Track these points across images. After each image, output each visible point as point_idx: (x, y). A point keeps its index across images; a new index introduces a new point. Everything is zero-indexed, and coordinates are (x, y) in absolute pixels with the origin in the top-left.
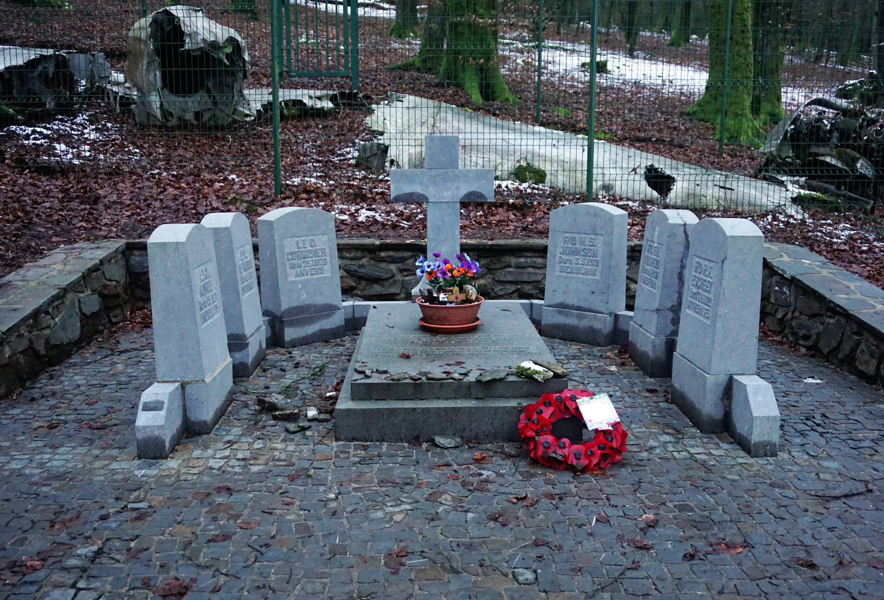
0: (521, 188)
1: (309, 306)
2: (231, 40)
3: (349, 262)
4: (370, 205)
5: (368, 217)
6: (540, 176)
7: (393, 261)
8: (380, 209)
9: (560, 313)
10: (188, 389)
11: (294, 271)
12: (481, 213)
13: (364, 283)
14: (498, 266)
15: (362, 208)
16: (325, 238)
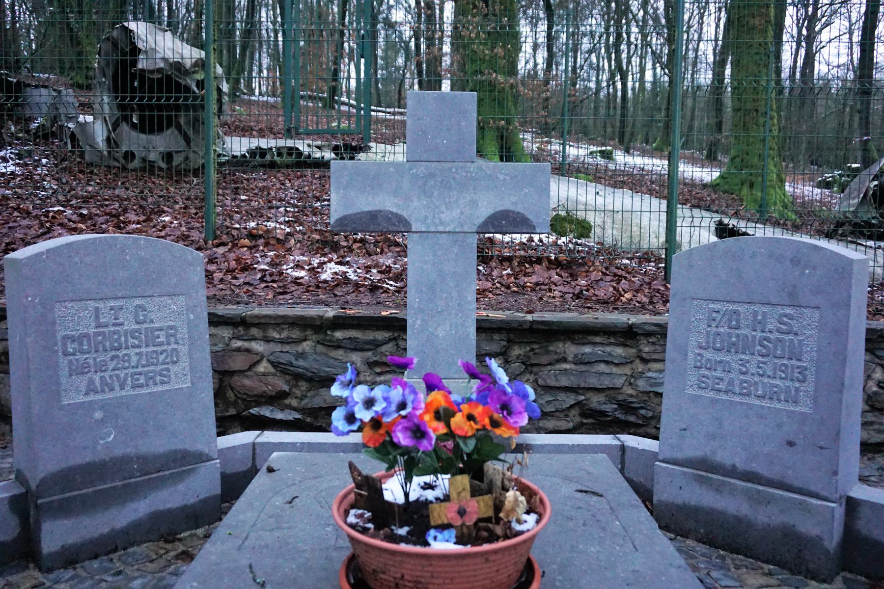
0: (559, 242)
1: (126, 460)
3: (278, 348)
4: (343, 257)
5: (336, 273)
6: (584, 229)
7: (357, 346)
8: (356, 262)
9: (701, 480)
11: (82, 382)
12: (509, 271)
13: (304, 385)
14: (544, 360)
15: (330, 261)
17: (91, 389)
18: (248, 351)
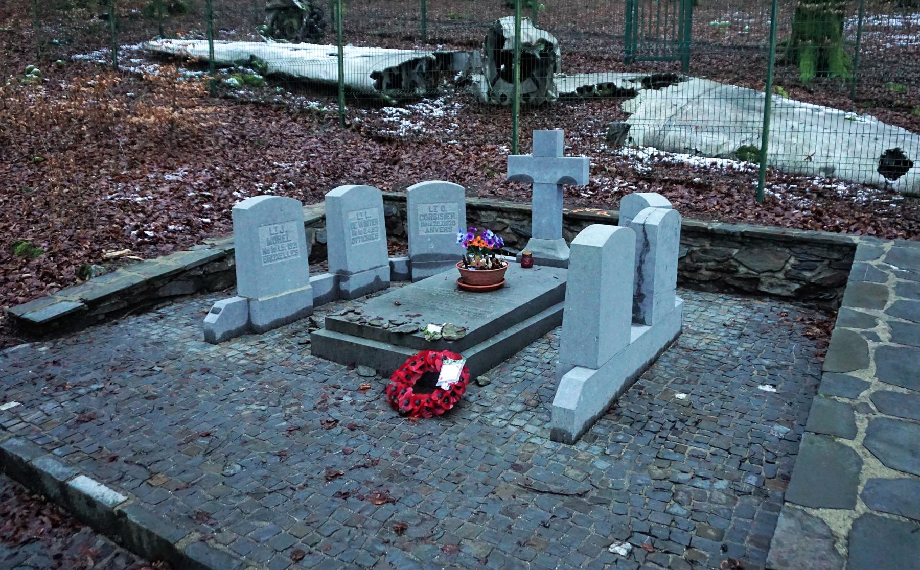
1: (437, 255)
2: (542, 41)
3: (514, 222)
10: (252, 303)
11: (424, 229)
16: (375, 210)
17: (427, 231)
18: (503, 223)
